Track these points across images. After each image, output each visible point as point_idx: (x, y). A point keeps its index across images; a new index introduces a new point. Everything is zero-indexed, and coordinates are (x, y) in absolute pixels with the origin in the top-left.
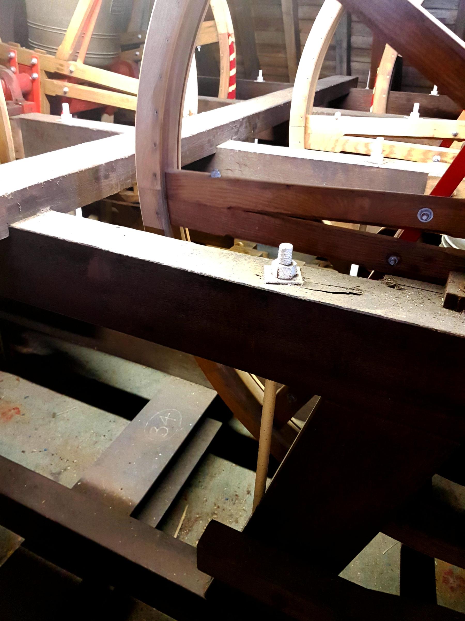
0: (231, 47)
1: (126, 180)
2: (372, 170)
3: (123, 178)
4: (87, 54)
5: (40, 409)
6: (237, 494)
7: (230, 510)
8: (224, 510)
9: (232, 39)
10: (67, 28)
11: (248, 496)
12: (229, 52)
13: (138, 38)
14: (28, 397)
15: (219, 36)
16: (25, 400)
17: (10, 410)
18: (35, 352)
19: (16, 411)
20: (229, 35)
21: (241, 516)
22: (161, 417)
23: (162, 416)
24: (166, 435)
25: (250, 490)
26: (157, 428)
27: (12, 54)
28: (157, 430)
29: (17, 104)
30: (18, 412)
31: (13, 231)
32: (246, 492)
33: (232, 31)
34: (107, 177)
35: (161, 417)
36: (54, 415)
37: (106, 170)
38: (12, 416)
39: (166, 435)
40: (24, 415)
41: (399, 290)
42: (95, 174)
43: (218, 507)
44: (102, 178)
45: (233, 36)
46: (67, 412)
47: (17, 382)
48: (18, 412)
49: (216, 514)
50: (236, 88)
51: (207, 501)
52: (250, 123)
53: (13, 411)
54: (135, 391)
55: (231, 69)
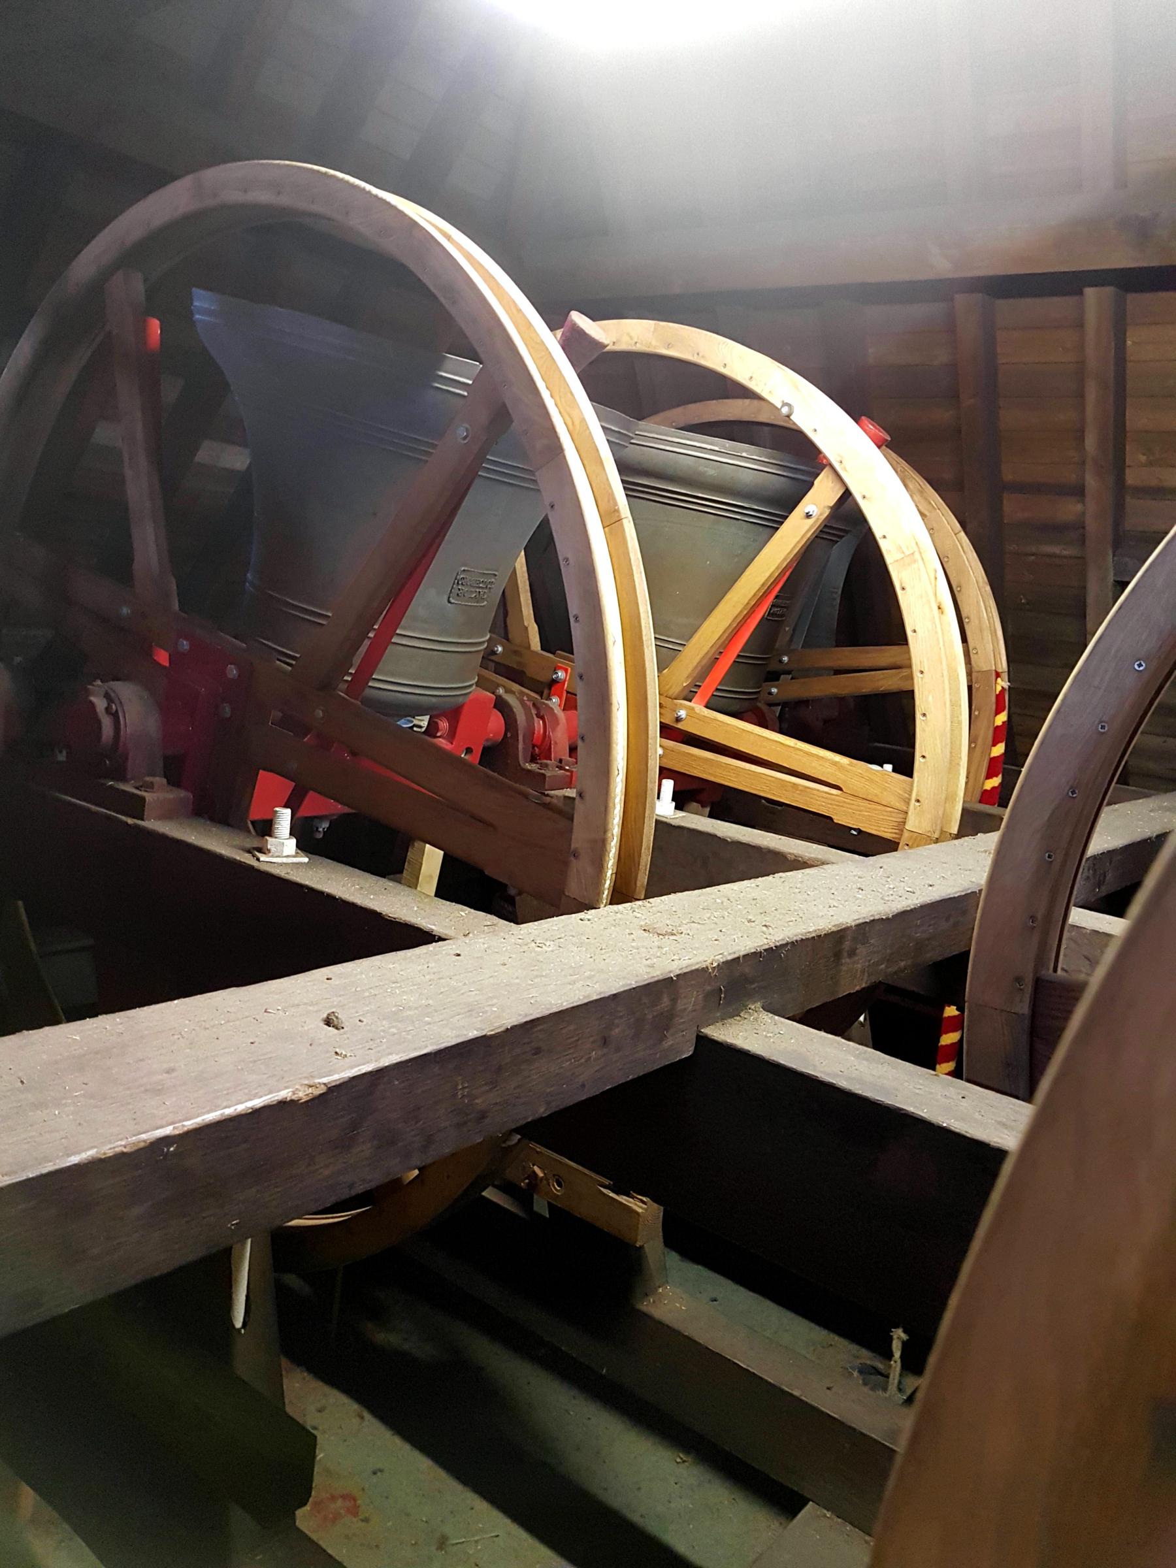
0: (999, 697)
1: (878, 964)
3: (875, 959)
4: (717, 690)
5: (408, 1515)
9: (1003, 683)
10: (688, 640)
12: (994, 707)
13: (781, 661)
14: (381, 1471)
15: (974, 675)
16: (374, 1479)
17: (333, 1498)
18: (406, 1346)
19: (348, 1504)
20: (998, 675)
27: (561, 674)
29: (561, 768)
30: (354, 1511)
31: (703, 1041)
33: (1003, 665)
34: (852, 953)
36: (443, 1542)
37: (854, 939)
38: (336, 1518)
40: (366, 1520)
42: (833, 945)
44: (845, 954)
45: (1006, 676)
46: (476, 1542)
47: (356, 1421)
48: (354, 1511)
50: (1001, 784)
52: (1095, 871)
53: (340, 1502)
54: (653, 1527)
55: (994, 745)
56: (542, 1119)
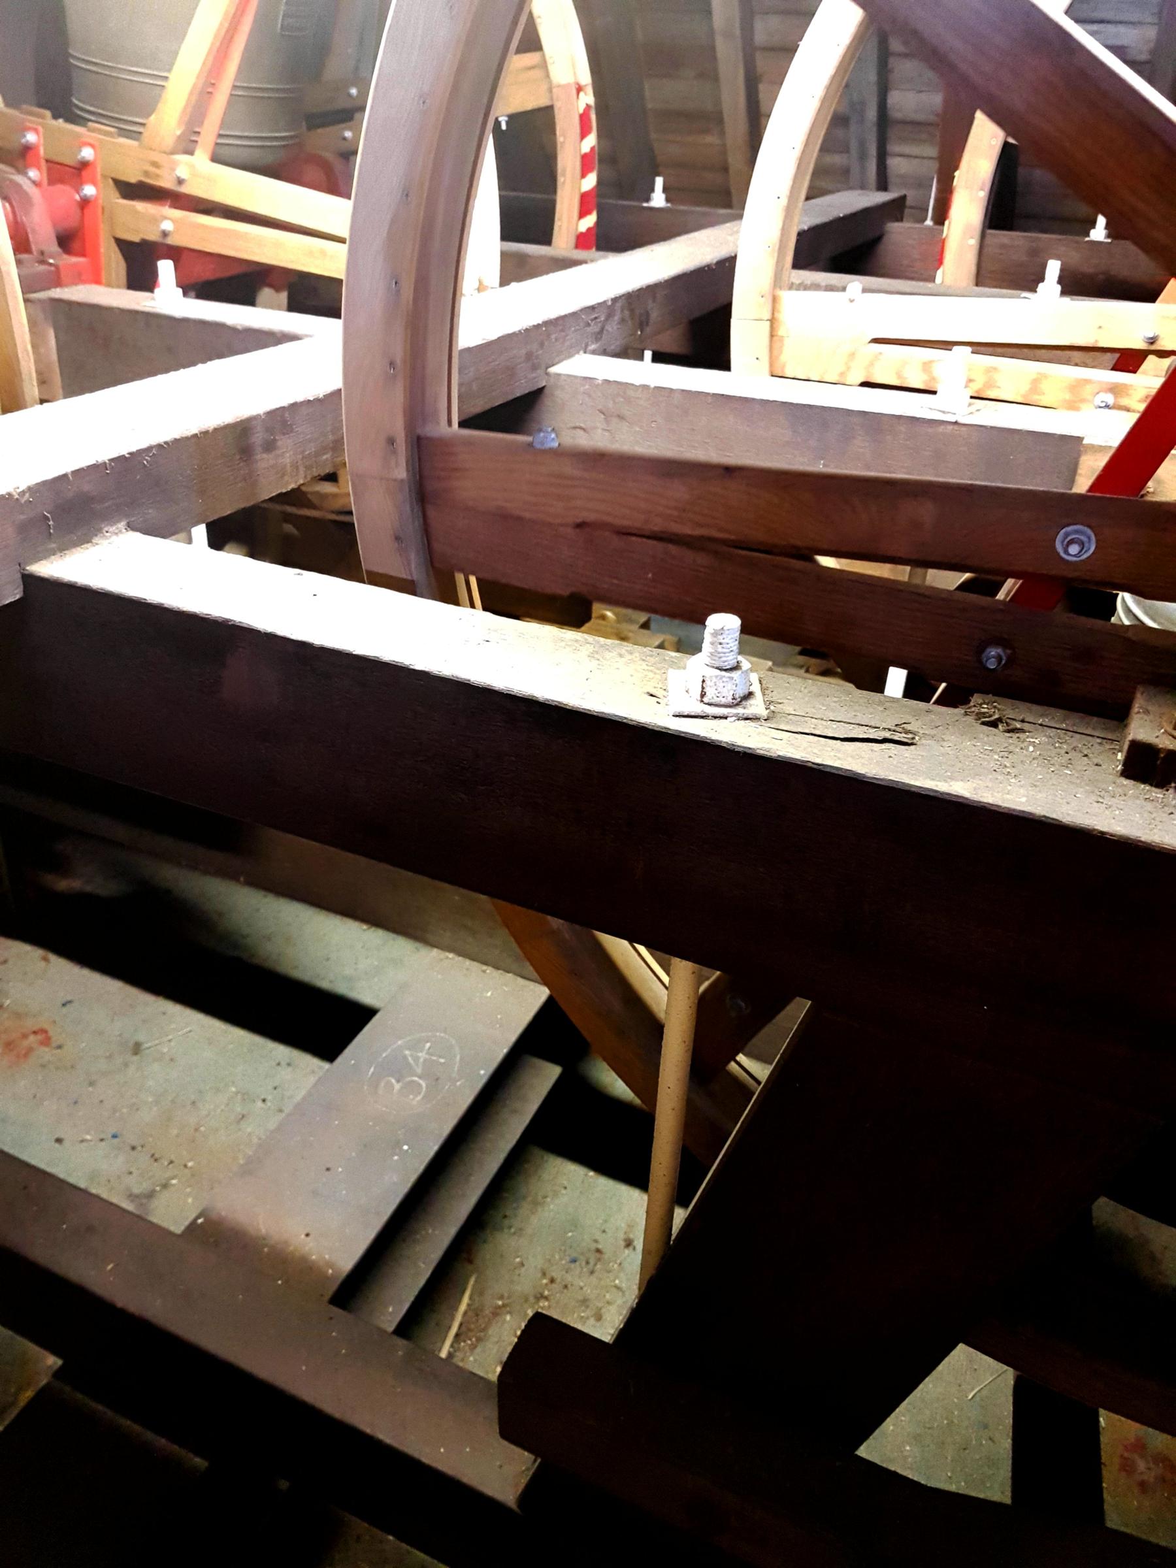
0: (584, 118)
1: (318, 454)
2: (941, 429)
3: (311, 449)
4: (220, 136)
5: (101, 1033)
6: (600, 1247)
7: (581, 1288)
8: (566, 1287)
9: (588, 98)
10: (169, 70)
11: (627, 1251)
12: (578, 130)
13: (350, 95)
14: (70, 1002)
15: (554, 90)
16: (64, 1010)
17: (25, 1036)
18: (88, 888)
19: (40, 1037)
20: (579, 89)
21: (608, 1303)
22: (407, 1052)
23: (409, 1049)
24: (419, 1098)
25: (631, 1236)
26: (398, 1081)
27: (31, 138)
28: (397, 1086)
29: (43, 262)
30: (47, 1042)
31: (32, 582)
32: (623, 1244)
33: (586, 78)
34: (270, 446)
35: (407, 1052)
36: (137, 1049)
37: (269, 430)
38: (30, 1050)
39: (419, 1098)
40: (59, 1047)
41: (1009, 731)
42: (239, 440)
43: (552, 1281)
44: (259, 449)
45: (590, 90)
46: (170, 1041)
47: (43, 964)
48: (47, 1042)
49: (546, 1298)
50: (598, 223)
51: (522, 1264)
52: (632, 311)
53: (32, 1038)
54: (341, 988)
55: (583, 175)
56: (1149, 479)
